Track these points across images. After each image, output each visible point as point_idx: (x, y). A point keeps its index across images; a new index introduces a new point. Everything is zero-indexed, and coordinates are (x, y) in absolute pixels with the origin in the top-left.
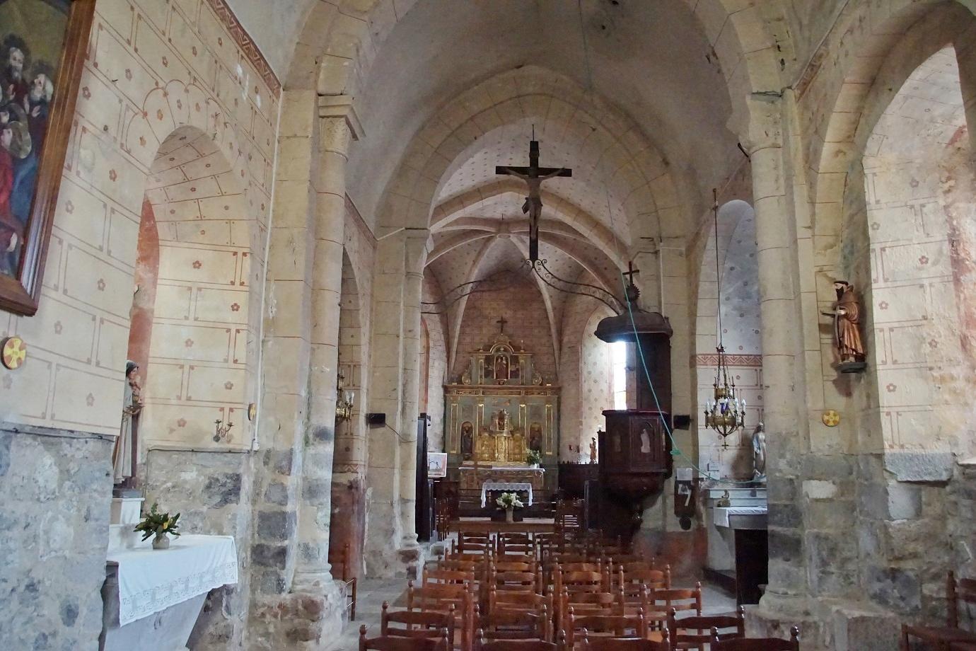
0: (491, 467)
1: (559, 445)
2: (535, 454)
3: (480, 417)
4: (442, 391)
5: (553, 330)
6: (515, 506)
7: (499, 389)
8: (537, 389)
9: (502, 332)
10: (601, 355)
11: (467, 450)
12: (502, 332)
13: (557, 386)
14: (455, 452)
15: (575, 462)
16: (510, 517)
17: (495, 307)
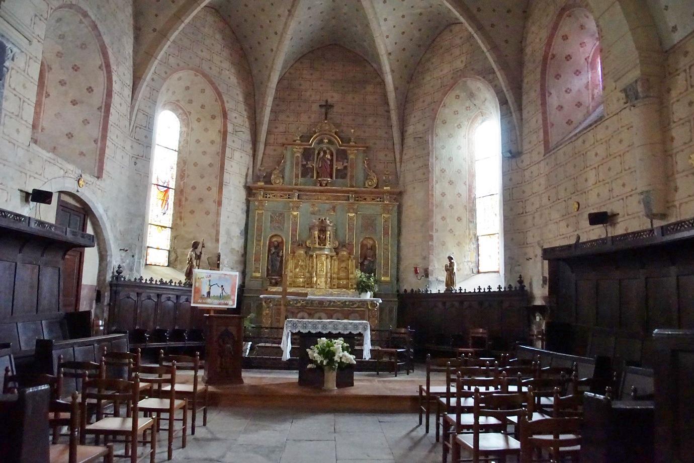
0: (306, 295)
1: (398, 269)
2: (369, 278)
3: (294, 230)
4: (243, 194)
5: (394, 116)
6: (341, 363)
7: (321, 192)
8: (372, 193)
9: (326, 119)
10: (459, 148)
11: (276, 272)
12: (326, 119)
13: (397, 190)
14: (258, 275)
15: (422, 290)
16: (331, 381)
17: (317, 88)
